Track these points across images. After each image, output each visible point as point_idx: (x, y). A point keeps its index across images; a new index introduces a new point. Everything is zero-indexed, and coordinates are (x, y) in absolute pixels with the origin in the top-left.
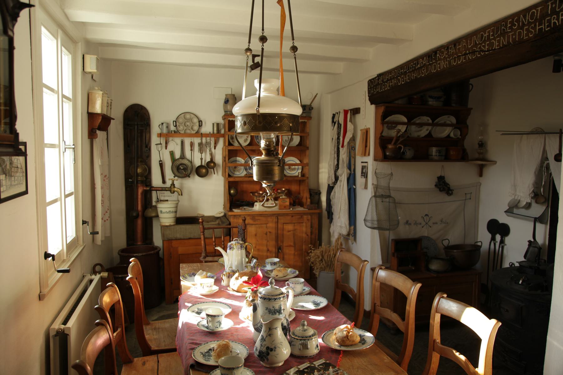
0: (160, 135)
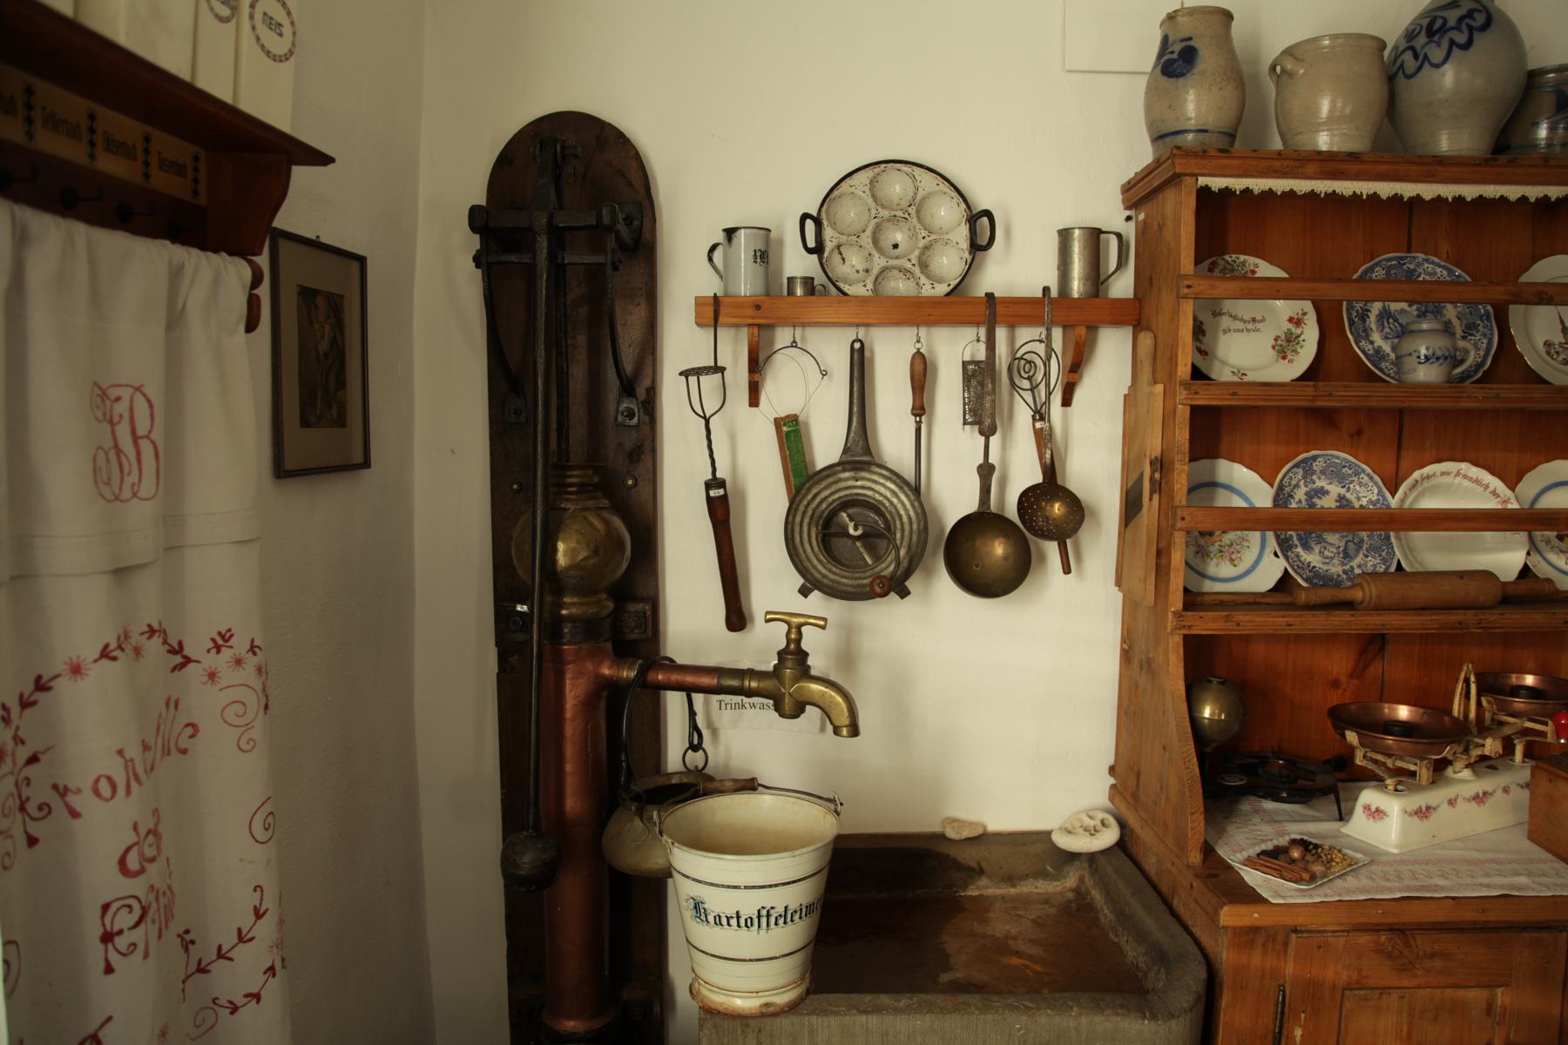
0: (713, 312)
